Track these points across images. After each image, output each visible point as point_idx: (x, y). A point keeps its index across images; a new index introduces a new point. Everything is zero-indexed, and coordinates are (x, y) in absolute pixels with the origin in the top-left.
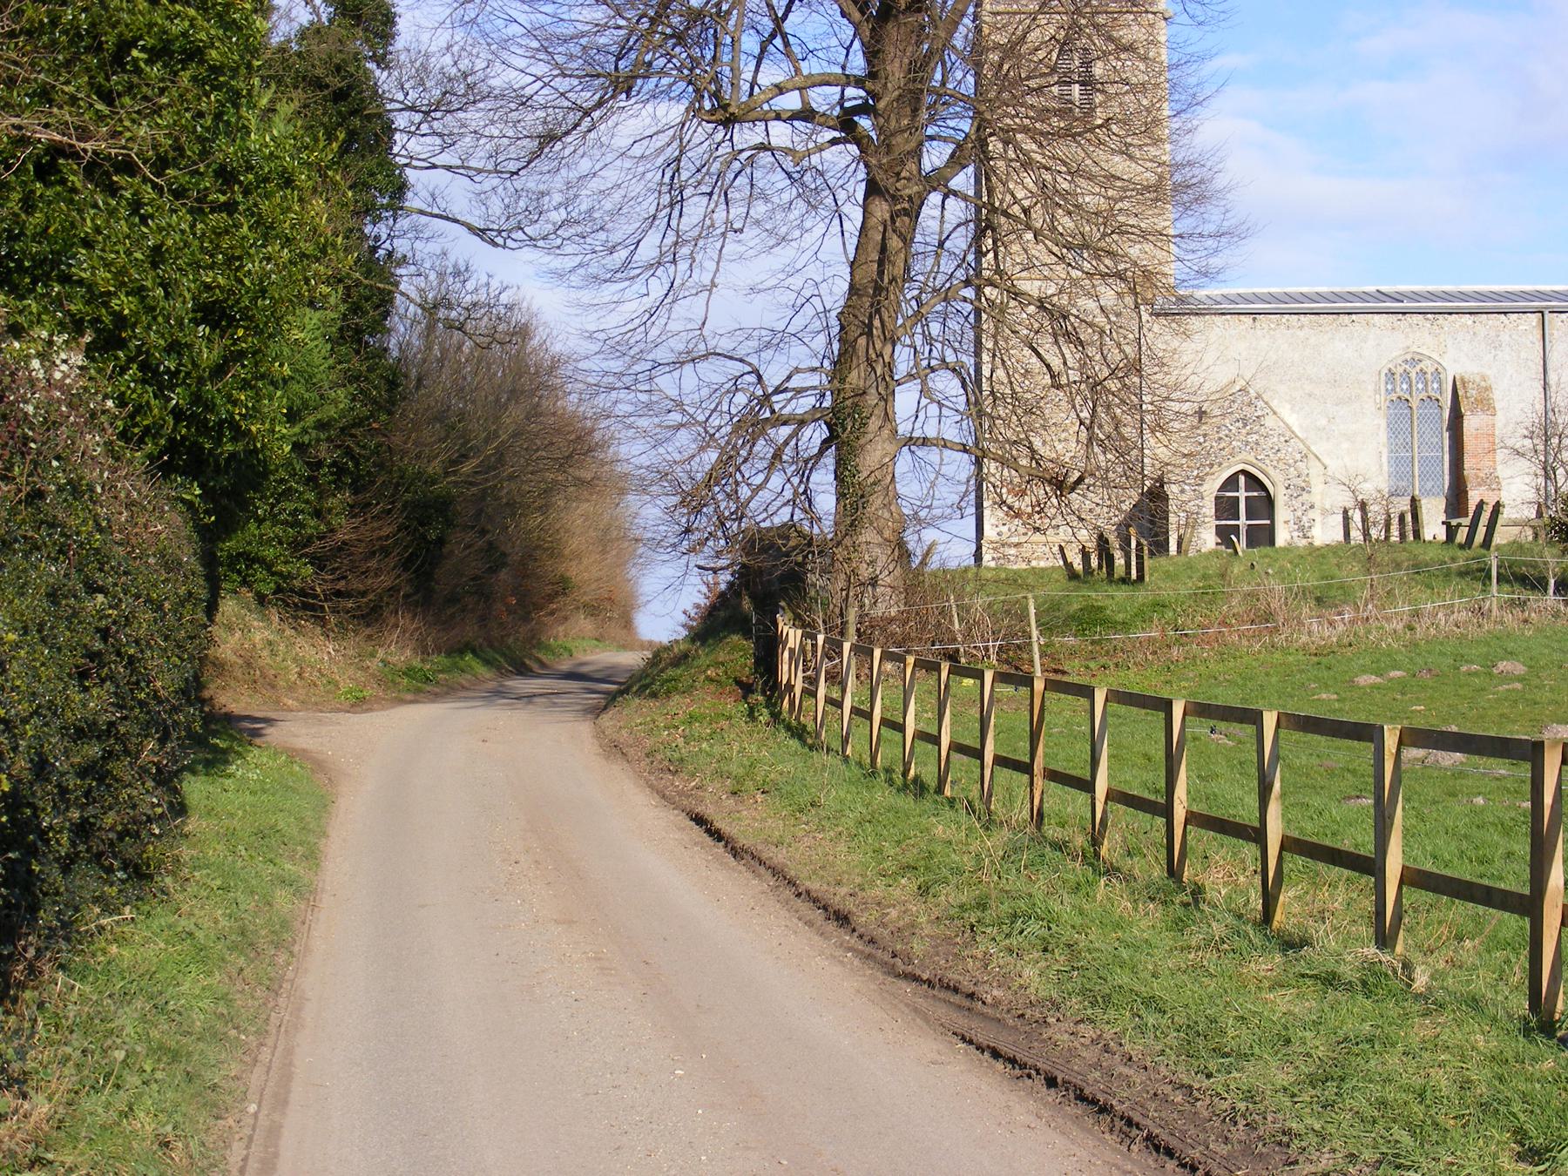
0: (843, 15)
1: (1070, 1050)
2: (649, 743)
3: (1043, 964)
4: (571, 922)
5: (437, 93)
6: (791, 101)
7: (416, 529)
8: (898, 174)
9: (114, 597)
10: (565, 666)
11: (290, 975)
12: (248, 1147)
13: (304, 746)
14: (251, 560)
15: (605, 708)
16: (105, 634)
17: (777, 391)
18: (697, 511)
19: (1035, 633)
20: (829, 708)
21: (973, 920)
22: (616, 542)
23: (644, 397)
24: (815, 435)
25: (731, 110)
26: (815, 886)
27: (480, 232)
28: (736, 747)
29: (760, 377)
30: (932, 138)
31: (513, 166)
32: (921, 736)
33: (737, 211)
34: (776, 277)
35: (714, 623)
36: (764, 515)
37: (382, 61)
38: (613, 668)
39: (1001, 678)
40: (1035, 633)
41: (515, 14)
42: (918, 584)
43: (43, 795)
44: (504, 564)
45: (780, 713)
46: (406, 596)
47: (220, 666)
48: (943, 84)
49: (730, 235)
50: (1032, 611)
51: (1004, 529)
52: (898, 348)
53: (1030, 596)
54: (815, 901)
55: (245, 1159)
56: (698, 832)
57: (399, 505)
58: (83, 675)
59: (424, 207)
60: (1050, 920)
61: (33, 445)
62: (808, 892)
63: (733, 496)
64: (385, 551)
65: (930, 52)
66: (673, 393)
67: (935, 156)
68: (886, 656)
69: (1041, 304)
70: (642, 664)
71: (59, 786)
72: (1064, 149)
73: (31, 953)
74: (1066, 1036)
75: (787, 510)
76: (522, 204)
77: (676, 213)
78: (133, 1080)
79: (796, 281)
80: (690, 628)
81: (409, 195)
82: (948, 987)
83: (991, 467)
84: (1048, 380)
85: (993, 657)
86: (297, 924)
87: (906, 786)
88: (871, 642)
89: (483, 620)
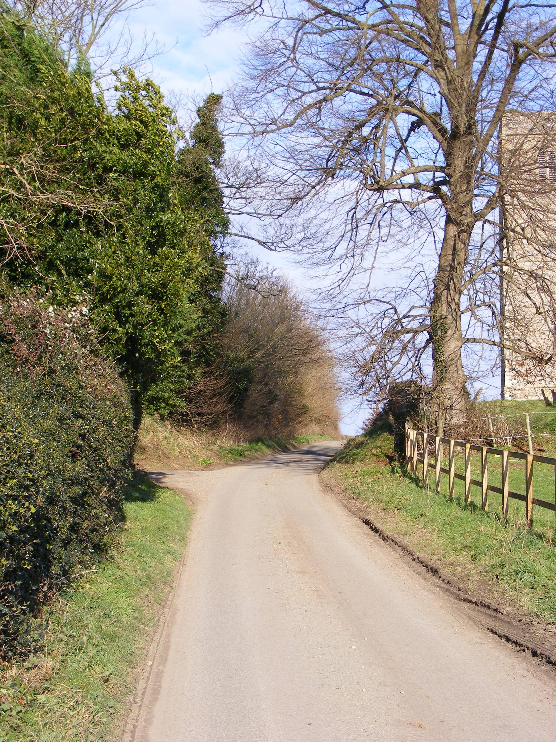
0: (434, 138)
1: (544, 638)
2: (344, 485)
3: (531, 595)
4: (304, 573)
5: (243, 179)
6: (409, 179)
7: (234, 384)
8: (461, 213)
9: (88, 420)
10: (305, 448)
11: (171, 597)
12: (147, 682)
13: (182, 487)
14: (158, 399)
15: (324, 468)
16: (83, 437)
17: (405, 317)
18: (367, 374)
19: (529, 432)
20: (430, 468)
21: (497, 573)
22: (330, 390)
23: (341, 321)
24: (424, 337)
25: (381, 183)
26: (421, 555)
27: (264, 244)
28: (385, 487)
29: (396, 310)
30: (477, 195)
31: (279, 212)
32: (474, 482)
33: (384, 231)
34: (402, 261)
35: (377, 427)
36: (399, 376)
37: (217, 165)
38: (328, 448)
39: (512, 454)
40: (529, 432)
41: (278, 142)
42: (472, 408)
43: (53, 512)
44: (276, 400)
45: (406, 471)
46: (230, 415)
47: (143, 449)
48: (482, 169)
49: (381, 243)
50: (528, 421)
51: (515, 381)
52: (462, 296)
53: (527, 414)
54: (422, 562)
55: (145, 688)
56: (367, 529)
57: (226, 372)
58: (74, 456)
59: (237, 232)
60: (535, 574)
61: (50, 348)
62: (418, 558)
63: (383, 367)
64: (220, 394)
65: (476, 155)
66: (355, 318)
67: (479, 204)
68: (456, 444)
69: (531, 274)
70: (342, 447)
71: (62, 506)
72: (541, 200)
73: (45, 589)
74: (542, 631)
75: (410, 374)
76: (283, 231)
77: (354, 232)
78: (92, 651)
79: (412, 264)
80: (365, 430)
81: (230, 226)
82: (485, 606)
83: (507, 353)
84: (534, 310)
85: (510, 443)
86: (174, 573)
87: (466, 506)
88: (450, 437)
89: (266, 426)
